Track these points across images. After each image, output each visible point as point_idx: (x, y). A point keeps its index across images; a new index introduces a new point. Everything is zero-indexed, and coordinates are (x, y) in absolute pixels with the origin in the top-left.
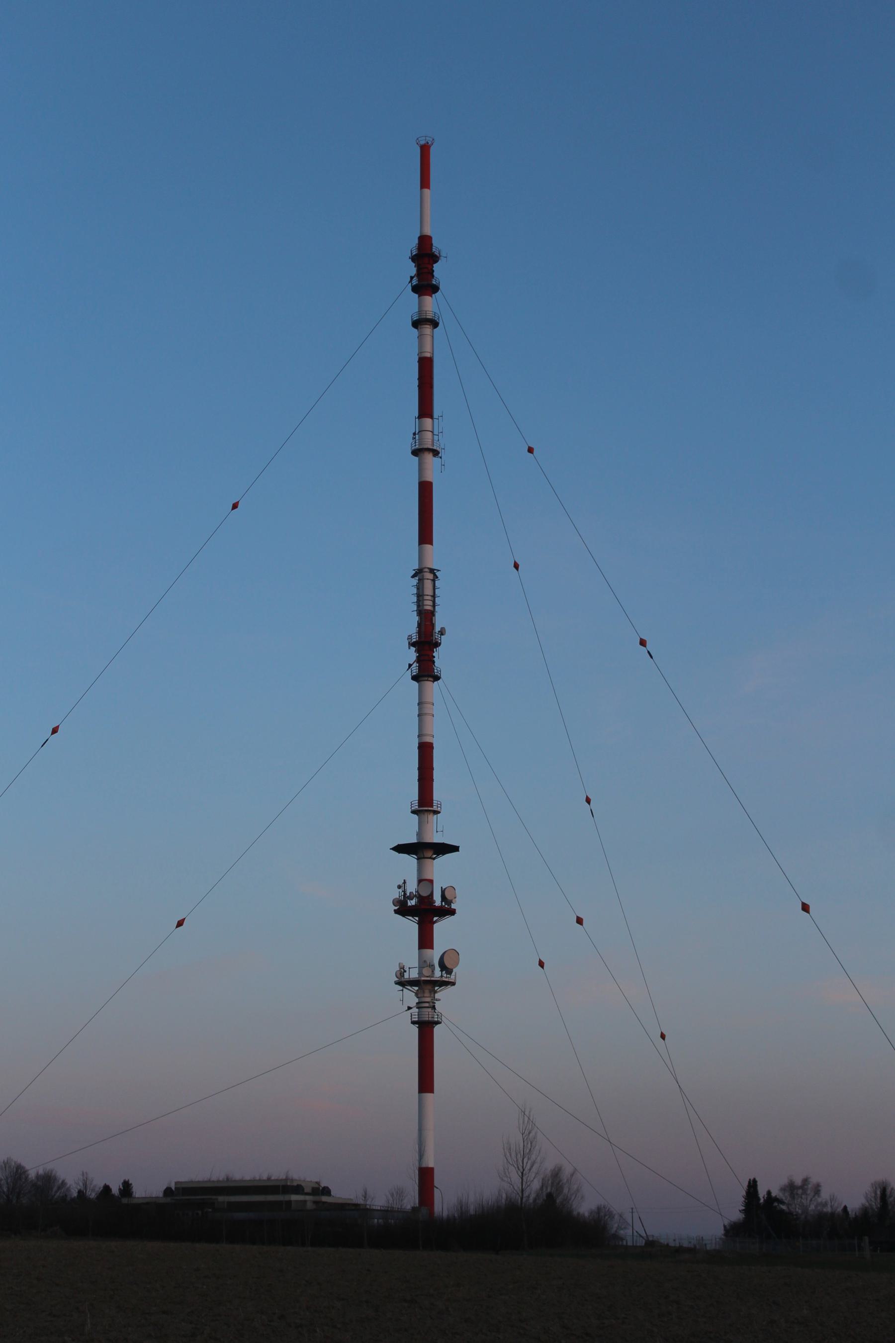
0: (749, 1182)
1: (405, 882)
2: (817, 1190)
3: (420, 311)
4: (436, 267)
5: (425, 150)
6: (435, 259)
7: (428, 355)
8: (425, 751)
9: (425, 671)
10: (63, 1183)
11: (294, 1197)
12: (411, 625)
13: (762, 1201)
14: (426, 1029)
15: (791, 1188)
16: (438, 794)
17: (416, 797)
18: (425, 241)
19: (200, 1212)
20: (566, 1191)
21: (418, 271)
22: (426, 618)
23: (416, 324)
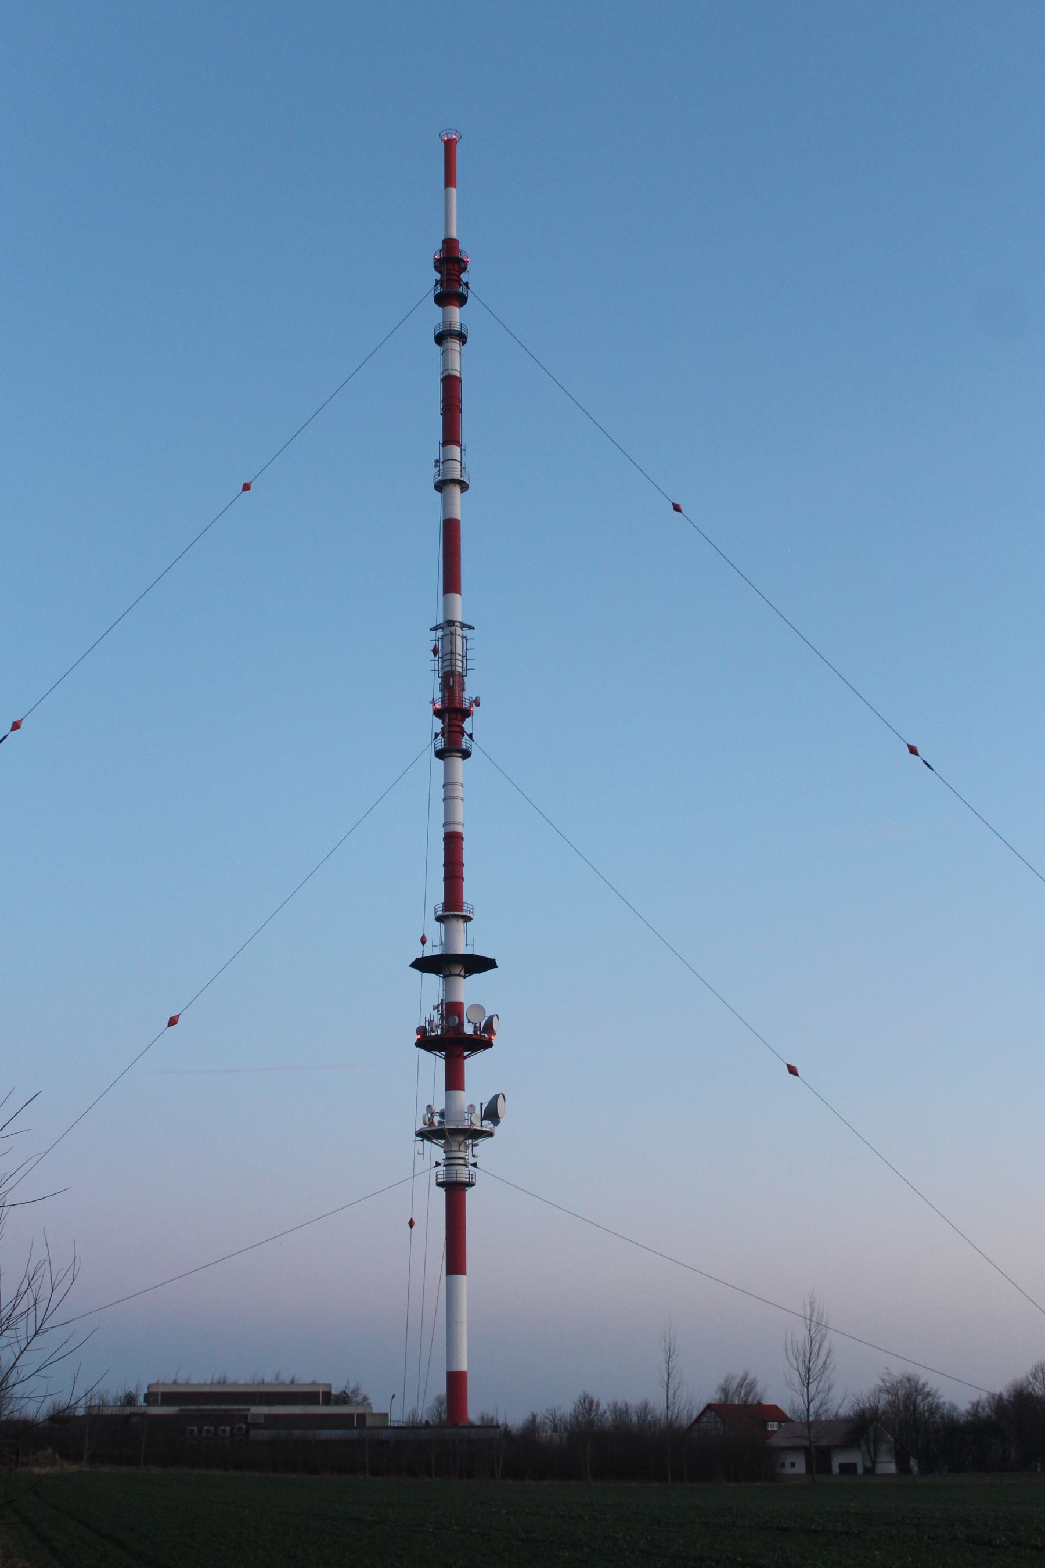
5: (449, 147)
8: (453, 842)
9: (452, 745)
12: (432, 690)
14: (455, 1191)
16: (470, 894)
18: (450, 244)
19: (228, 1429)
22: (451, 681)
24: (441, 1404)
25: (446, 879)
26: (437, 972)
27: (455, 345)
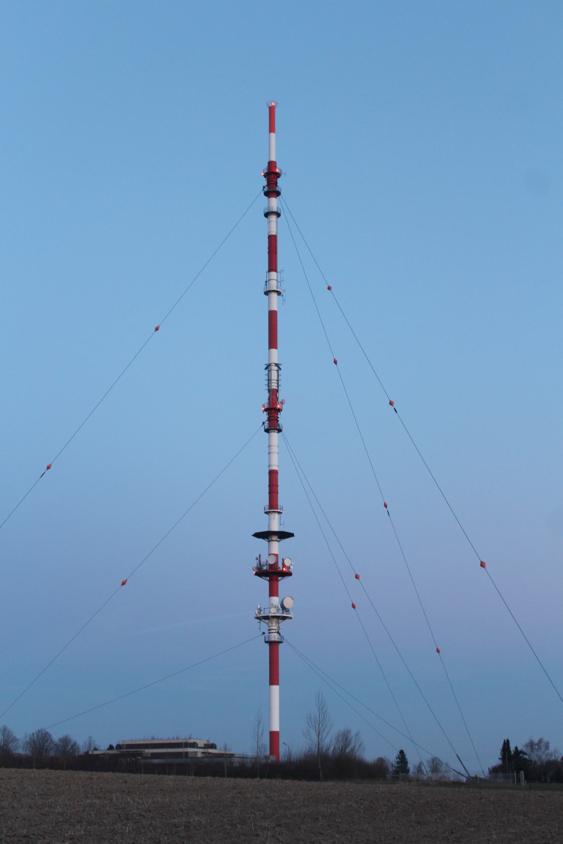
0: (504, 742)
1: (260, 556)
2: (547, 746)
3: (269, 207)
4: (279, 180)
5: (272, 110)
6: (278, 175)
7: (274, 234)
10: (75, 743)
11: (190, 750)
12: (264, 398)
13: (512, 753)
15: (531, 744)
16: (281, 500)
17: (267, 503)
19: (129, 760)
20: (352, 745)
21: (268, 182)
23: (267, 215)
24: (26, 737)
25: (269, 253)
26: (263, 538)
27: (274, 296)
